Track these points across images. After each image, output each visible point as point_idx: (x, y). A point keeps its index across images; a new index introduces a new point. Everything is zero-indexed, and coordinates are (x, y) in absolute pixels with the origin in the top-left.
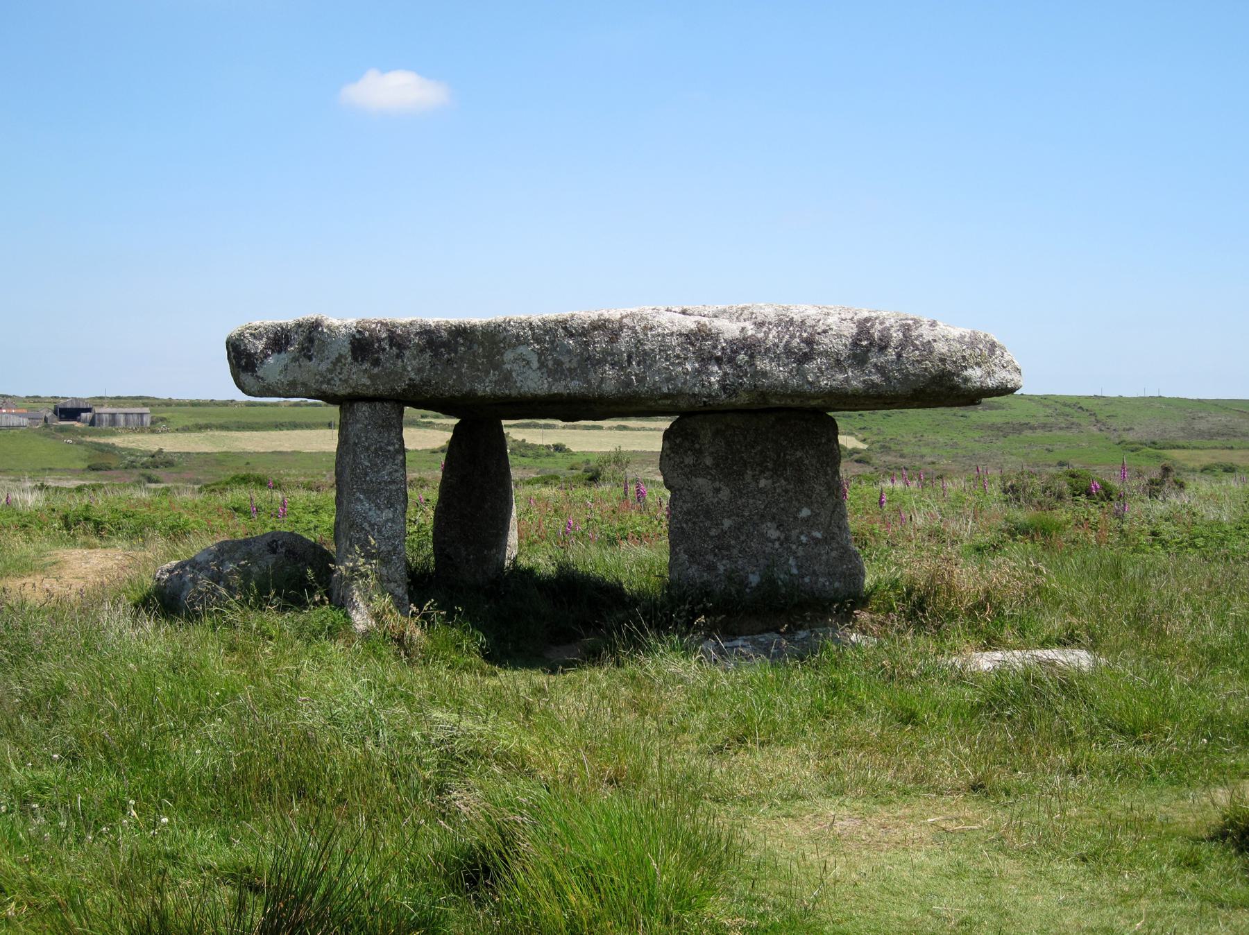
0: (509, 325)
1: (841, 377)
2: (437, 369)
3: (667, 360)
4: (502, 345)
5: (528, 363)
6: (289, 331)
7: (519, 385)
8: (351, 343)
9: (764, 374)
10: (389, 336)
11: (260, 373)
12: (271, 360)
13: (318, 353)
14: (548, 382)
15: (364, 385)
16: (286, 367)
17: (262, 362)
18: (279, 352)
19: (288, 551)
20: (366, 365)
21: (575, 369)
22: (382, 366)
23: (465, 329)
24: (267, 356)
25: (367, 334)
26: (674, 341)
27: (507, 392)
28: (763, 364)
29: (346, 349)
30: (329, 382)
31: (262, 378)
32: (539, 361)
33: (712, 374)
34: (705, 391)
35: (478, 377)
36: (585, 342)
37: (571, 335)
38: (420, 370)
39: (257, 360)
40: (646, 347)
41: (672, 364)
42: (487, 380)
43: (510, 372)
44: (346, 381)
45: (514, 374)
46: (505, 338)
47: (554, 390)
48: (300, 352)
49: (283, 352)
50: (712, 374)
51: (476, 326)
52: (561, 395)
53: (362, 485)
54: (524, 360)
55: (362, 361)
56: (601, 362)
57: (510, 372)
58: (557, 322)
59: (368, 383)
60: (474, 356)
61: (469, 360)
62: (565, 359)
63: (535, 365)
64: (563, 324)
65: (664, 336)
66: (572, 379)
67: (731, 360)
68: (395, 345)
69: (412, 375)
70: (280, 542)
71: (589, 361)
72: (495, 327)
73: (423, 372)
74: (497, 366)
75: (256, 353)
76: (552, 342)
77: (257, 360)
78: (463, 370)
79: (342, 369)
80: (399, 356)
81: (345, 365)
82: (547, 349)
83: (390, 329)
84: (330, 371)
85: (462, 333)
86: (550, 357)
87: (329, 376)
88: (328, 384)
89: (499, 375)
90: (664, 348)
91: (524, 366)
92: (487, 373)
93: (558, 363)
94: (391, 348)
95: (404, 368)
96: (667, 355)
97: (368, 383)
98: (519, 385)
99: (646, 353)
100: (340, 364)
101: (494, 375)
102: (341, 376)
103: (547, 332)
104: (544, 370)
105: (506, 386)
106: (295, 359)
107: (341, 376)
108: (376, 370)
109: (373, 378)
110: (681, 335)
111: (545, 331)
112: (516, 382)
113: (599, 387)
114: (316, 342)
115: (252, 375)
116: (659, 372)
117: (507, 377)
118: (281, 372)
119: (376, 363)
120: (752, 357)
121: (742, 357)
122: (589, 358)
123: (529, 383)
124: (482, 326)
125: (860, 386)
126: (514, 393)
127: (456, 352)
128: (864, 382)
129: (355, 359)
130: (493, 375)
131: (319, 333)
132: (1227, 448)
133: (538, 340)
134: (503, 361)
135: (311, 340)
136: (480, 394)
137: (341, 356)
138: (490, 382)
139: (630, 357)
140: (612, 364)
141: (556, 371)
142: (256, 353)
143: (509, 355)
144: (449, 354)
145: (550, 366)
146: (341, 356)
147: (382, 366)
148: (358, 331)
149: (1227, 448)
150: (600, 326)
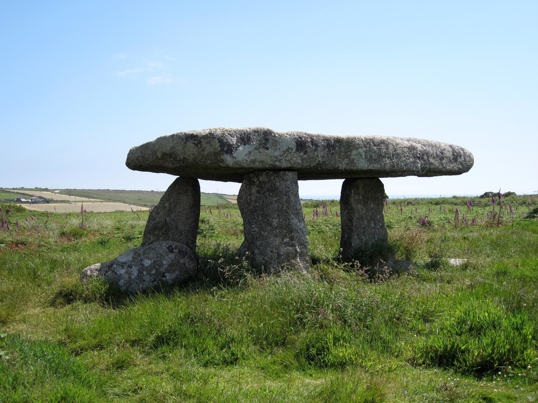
0: (356, 139)
1: (452, 165)
2: (329, 157)
3: (405, 157)
4: (352, 148)
5: (361, 156)
6: (249, 134)
7: (357, 165)
8: (296, 142)
9: (432, 164)
10: (311, 141)
11: (235, 155)
12: (241, 148)
13: (272, 146)
14: (368, 164)
15: (298, 163)
16: (250, 153)
17: (236, 149)
18: (245, 145)
19: (179, 251)
20: (302, 154)
21: (376, 159)
22: (308, 154)
23: (340, 140)
24: (238, 146)
25: (303, 139)
26: (406, 150)
27: (352, 168)
28: (431, 160)
29: (293, 146)
30: (280, 161)
31: (235, 158)
32: (365, 155)
33: (418, 163)
34: (417, 170)
35: (340, 161)
36: (380, 148)
37: (375, 145)
38: (323, 157)
39: (234, 148)
40: (398, 152)
41: (406, 159)
42: (343, 163)
43: (354, 160)
44: (289, 161)
45: (355, 161)
46: (354, 145)
47: (370, 168)
48: (260, 145)
49: (247, 145)
50: (418, 163)
51: (343, 138)
52: (371, 170)
53: (293, 211)
54: (360, 154)
55: (300, 151)
56: (385, 157)
57: (354, 160)
58: (370, 139)
59: (300, 162)
60: (341, 152)
61: (339, 153)
62: (373, 155)
63: (364, 157)
64: (372, 140)
65: (402, 148)
66: (375, 163)
67: (423, 158)
68: (314, 145)
69: (320, 159)
70: (173, 246)
71: (381, 156)
72: (351, 140)
73: (324, 158)
74: (348, 157)
75: (233, 144)
76: (370, 148)
77: (234, 148)
78: (336, 158)
79: (287, 155)
80: (315, 150)
81: (291, 153)
82: (368, 150)
83: (311, 137)
84: (281, 156)
85: (338, 141)
86: (368, 154)
87: (280, 158)
88: (279, 162)
89: (349, 160)
90: (403, 152)
91: (360, 157)
92: (344, 159)
93: (371, 156)
94: (312, 146)
95: (317, 156)
96: (405, 155)
97: (300, 162)
98: (357, 165)
99: (398, 154)
100: (287, 152)
101: (346, 160)
102: (286, 158)
103: (368, 143)
104: (367, 159)
105: (352, 166)
106: (256, 149)
107: (286, 158)
108: (305, 156)
109: (303, 160)
110: (407, 147)
111: (367, 143)
112: (356, 164)
113: (384, 167)
114: (270, 141)
115: (231, 156)
116: (403, 162)
117: (352, 161)
118: (247, 155)
119: (305, 153)
120: (428, 157)
121: (425, 157)
122: (381, 155)
123: (361, 164)
124: (346, 139)
125: (457, 169)
126: (355, 168)
127: (335, 150)
128: (458, 167)
129: (297, 150)
130: (346, 161)
131: (273, 136)
132: (118, 201)
133: (365, 147)
134: (351, 154)
135: (267, 140)
136: (340, 168)
137: (289, 148)
138: (345, 163)
139: (393, 155)
140: (388, 158)
141: (370, 160)
142: (233, 144)
143: (354, 152)
144: (333, 150)
145: (368, 158)
146: (289, 148)
147: (308, 154)
148: (299, 137)
149: (118, 201)
150: (383, 142)
